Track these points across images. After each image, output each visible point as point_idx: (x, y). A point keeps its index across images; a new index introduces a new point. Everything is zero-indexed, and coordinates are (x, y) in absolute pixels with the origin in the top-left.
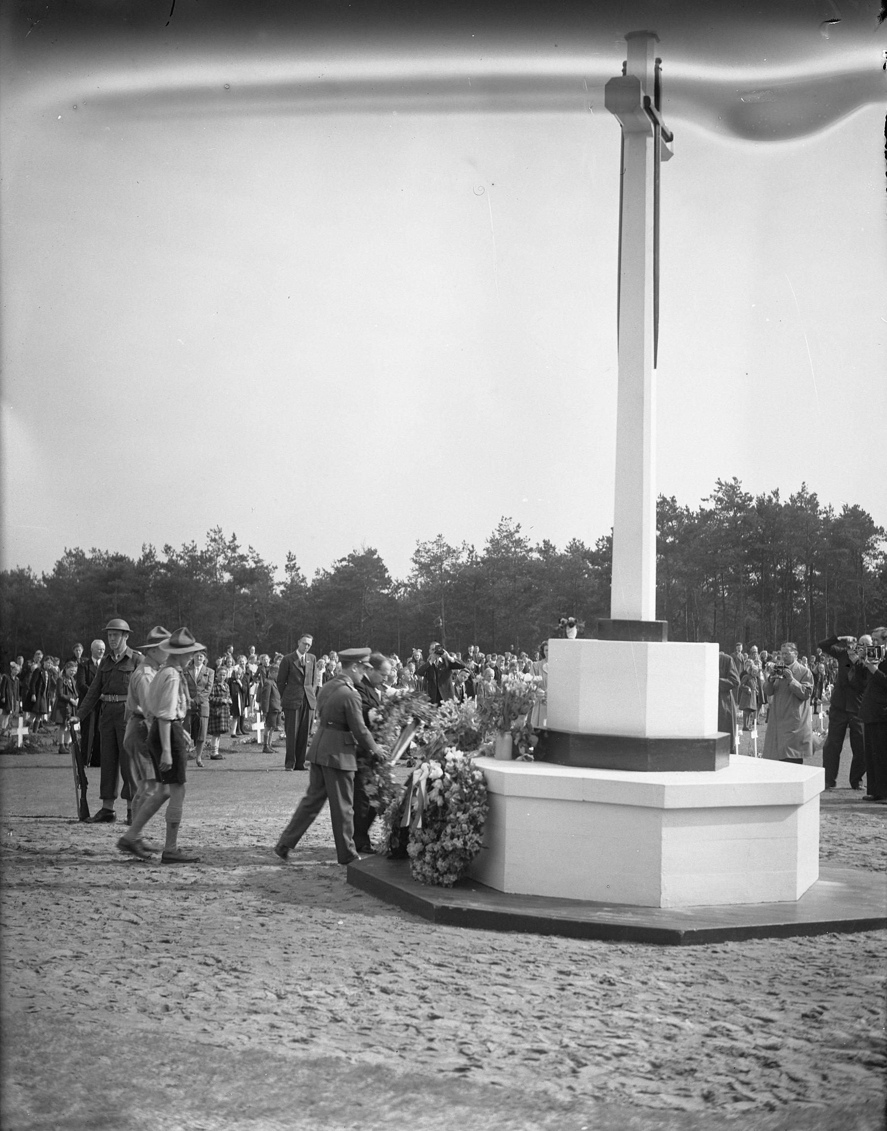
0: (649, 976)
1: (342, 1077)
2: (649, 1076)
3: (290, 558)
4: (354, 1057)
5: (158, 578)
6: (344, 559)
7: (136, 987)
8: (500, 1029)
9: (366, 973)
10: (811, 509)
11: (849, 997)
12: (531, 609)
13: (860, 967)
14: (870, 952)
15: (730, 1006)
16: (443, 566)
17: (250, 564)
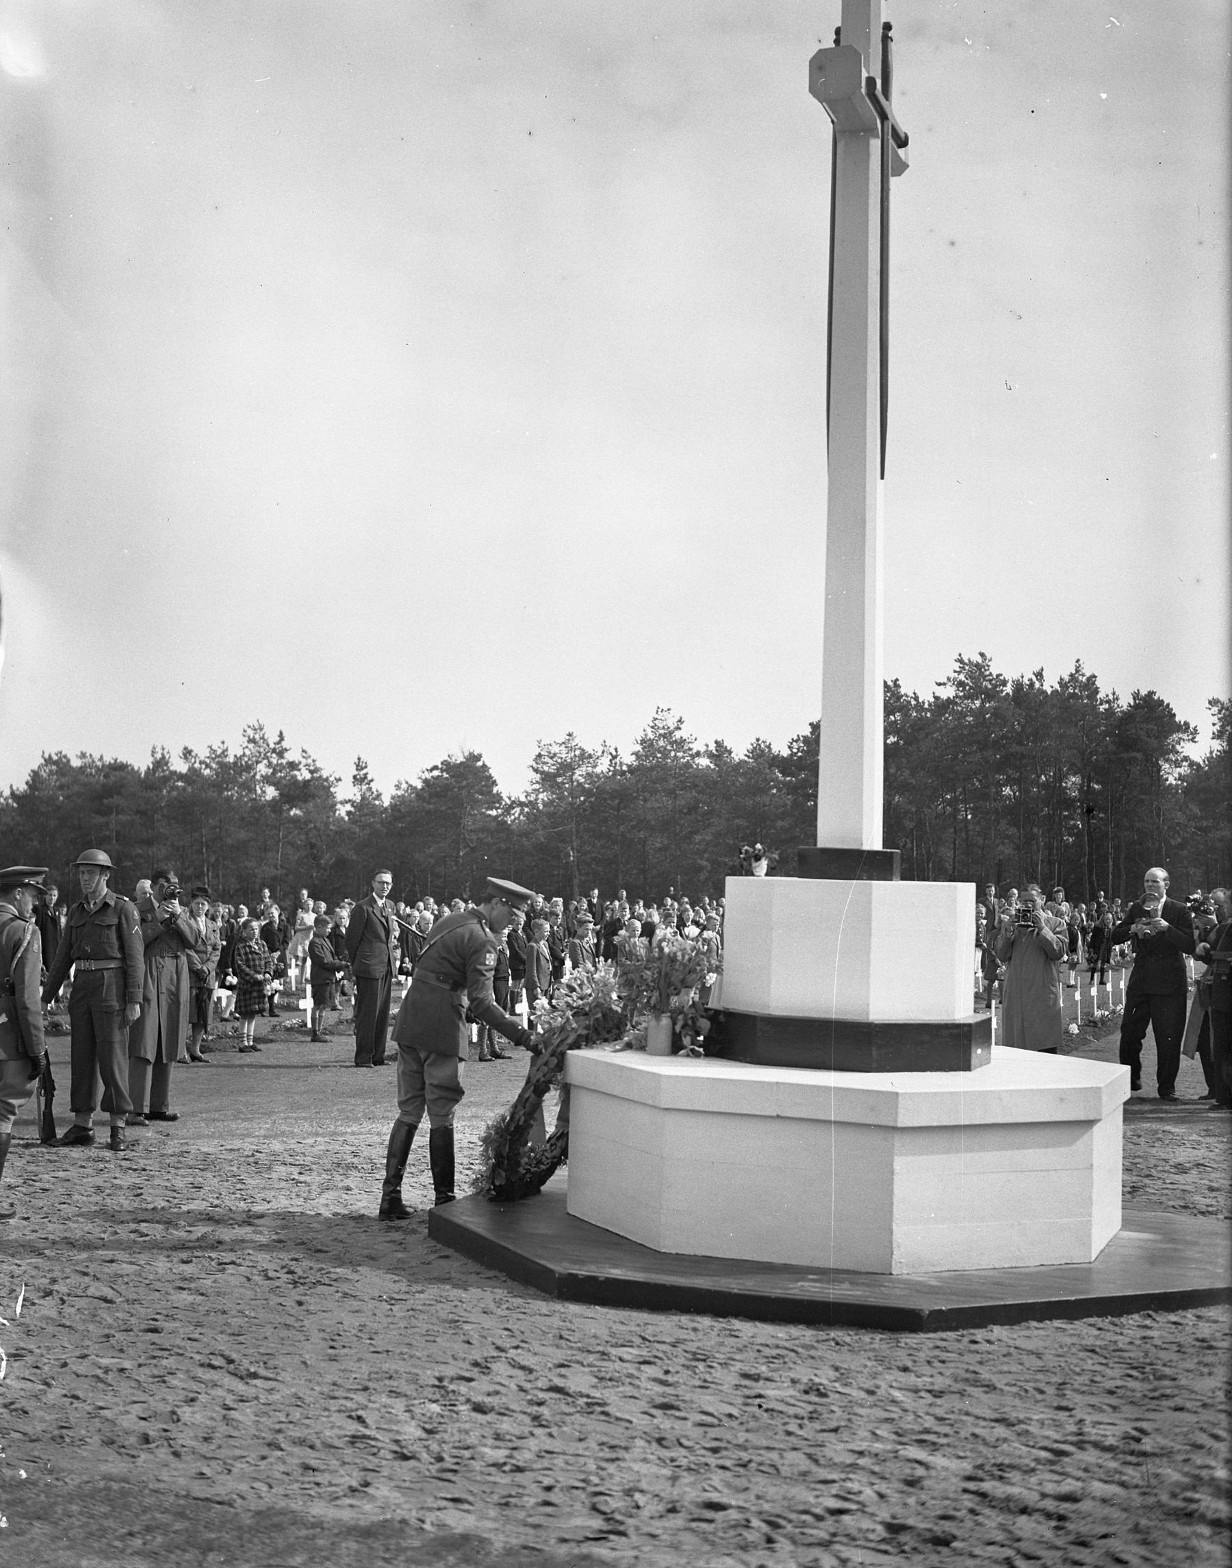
1: (409, 1553)
2: (883, 1547)
3: (359, 767)
4: (430, 1517)
5: (174, 793)
6: (435, 768)
7: (101, 1404)
8: (654, 1469)
9: (452, 1380)
10: (1088, 697)
11: (1178, 1413)
12: (698, 838)
13: (1190, 1364)
14: (1203, 1340)
15: (1001, 1431)
17: (303, 775)
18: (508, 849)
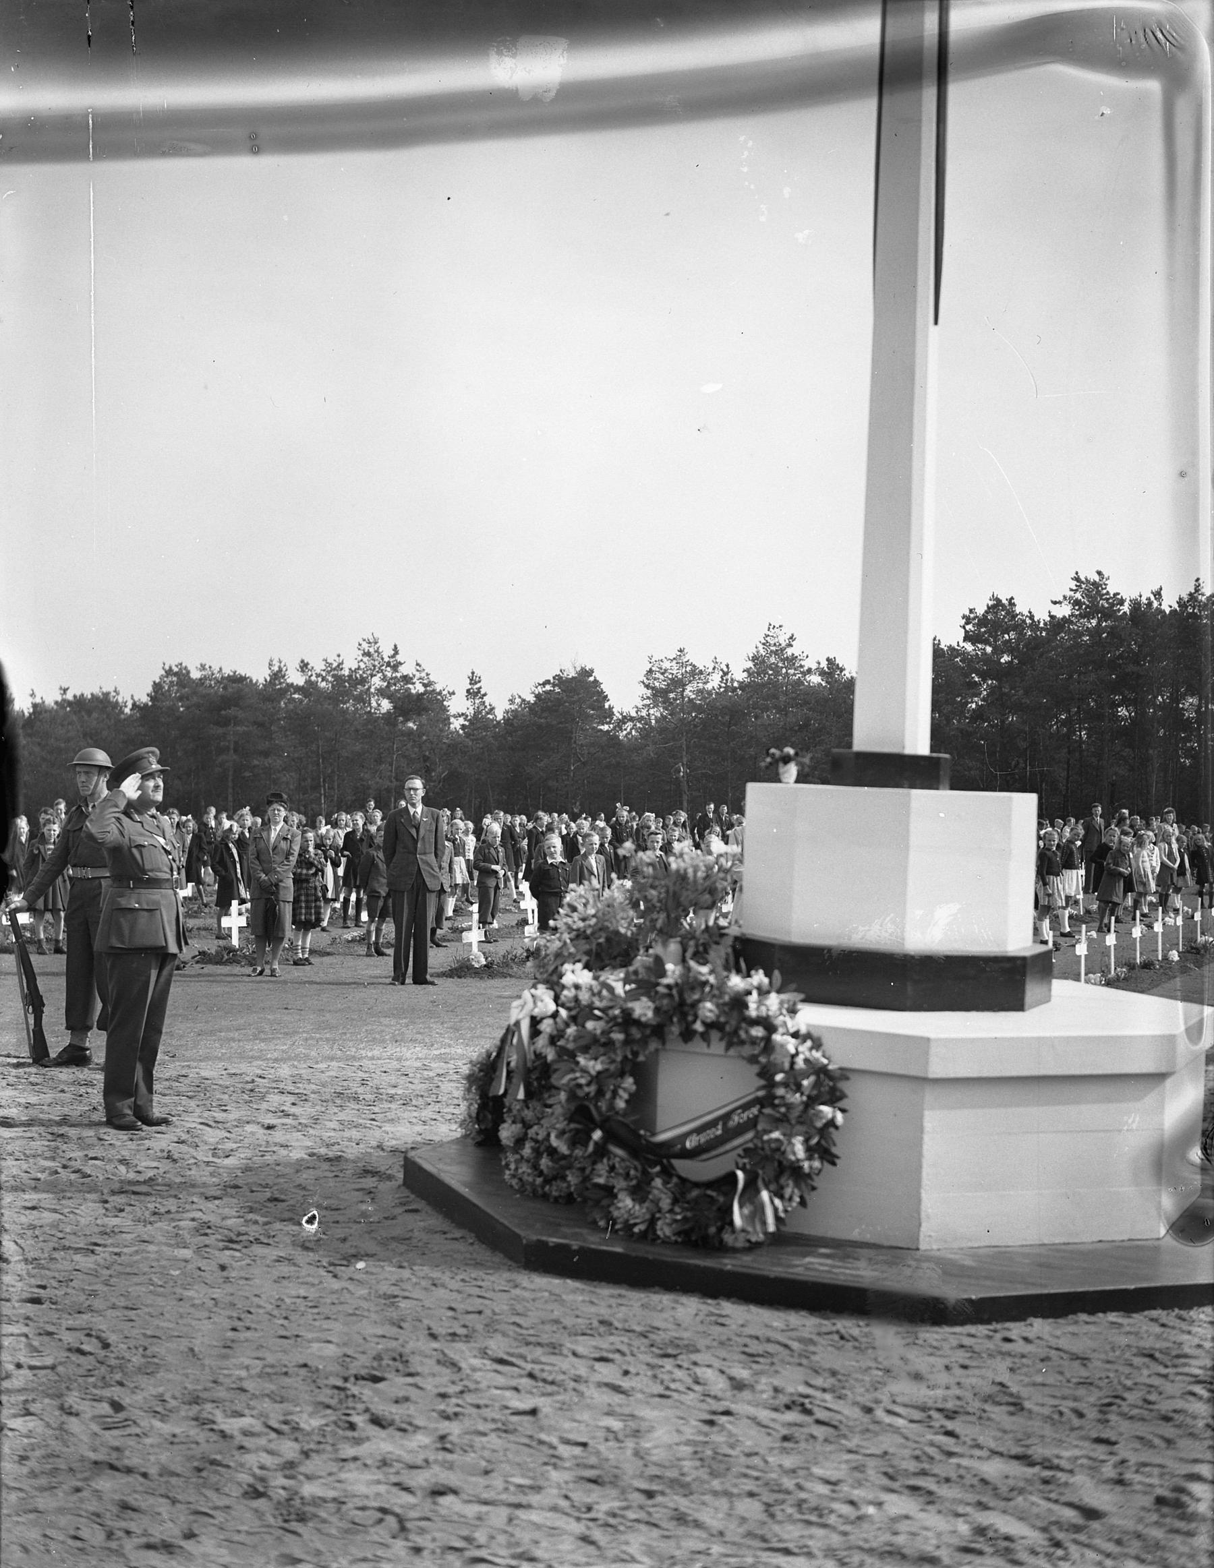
0: (878, 1395)
3: (474, 680)
6: (548, 682)
16: (687, 693)
17: (418, 688)
18: (618, 763)
